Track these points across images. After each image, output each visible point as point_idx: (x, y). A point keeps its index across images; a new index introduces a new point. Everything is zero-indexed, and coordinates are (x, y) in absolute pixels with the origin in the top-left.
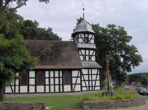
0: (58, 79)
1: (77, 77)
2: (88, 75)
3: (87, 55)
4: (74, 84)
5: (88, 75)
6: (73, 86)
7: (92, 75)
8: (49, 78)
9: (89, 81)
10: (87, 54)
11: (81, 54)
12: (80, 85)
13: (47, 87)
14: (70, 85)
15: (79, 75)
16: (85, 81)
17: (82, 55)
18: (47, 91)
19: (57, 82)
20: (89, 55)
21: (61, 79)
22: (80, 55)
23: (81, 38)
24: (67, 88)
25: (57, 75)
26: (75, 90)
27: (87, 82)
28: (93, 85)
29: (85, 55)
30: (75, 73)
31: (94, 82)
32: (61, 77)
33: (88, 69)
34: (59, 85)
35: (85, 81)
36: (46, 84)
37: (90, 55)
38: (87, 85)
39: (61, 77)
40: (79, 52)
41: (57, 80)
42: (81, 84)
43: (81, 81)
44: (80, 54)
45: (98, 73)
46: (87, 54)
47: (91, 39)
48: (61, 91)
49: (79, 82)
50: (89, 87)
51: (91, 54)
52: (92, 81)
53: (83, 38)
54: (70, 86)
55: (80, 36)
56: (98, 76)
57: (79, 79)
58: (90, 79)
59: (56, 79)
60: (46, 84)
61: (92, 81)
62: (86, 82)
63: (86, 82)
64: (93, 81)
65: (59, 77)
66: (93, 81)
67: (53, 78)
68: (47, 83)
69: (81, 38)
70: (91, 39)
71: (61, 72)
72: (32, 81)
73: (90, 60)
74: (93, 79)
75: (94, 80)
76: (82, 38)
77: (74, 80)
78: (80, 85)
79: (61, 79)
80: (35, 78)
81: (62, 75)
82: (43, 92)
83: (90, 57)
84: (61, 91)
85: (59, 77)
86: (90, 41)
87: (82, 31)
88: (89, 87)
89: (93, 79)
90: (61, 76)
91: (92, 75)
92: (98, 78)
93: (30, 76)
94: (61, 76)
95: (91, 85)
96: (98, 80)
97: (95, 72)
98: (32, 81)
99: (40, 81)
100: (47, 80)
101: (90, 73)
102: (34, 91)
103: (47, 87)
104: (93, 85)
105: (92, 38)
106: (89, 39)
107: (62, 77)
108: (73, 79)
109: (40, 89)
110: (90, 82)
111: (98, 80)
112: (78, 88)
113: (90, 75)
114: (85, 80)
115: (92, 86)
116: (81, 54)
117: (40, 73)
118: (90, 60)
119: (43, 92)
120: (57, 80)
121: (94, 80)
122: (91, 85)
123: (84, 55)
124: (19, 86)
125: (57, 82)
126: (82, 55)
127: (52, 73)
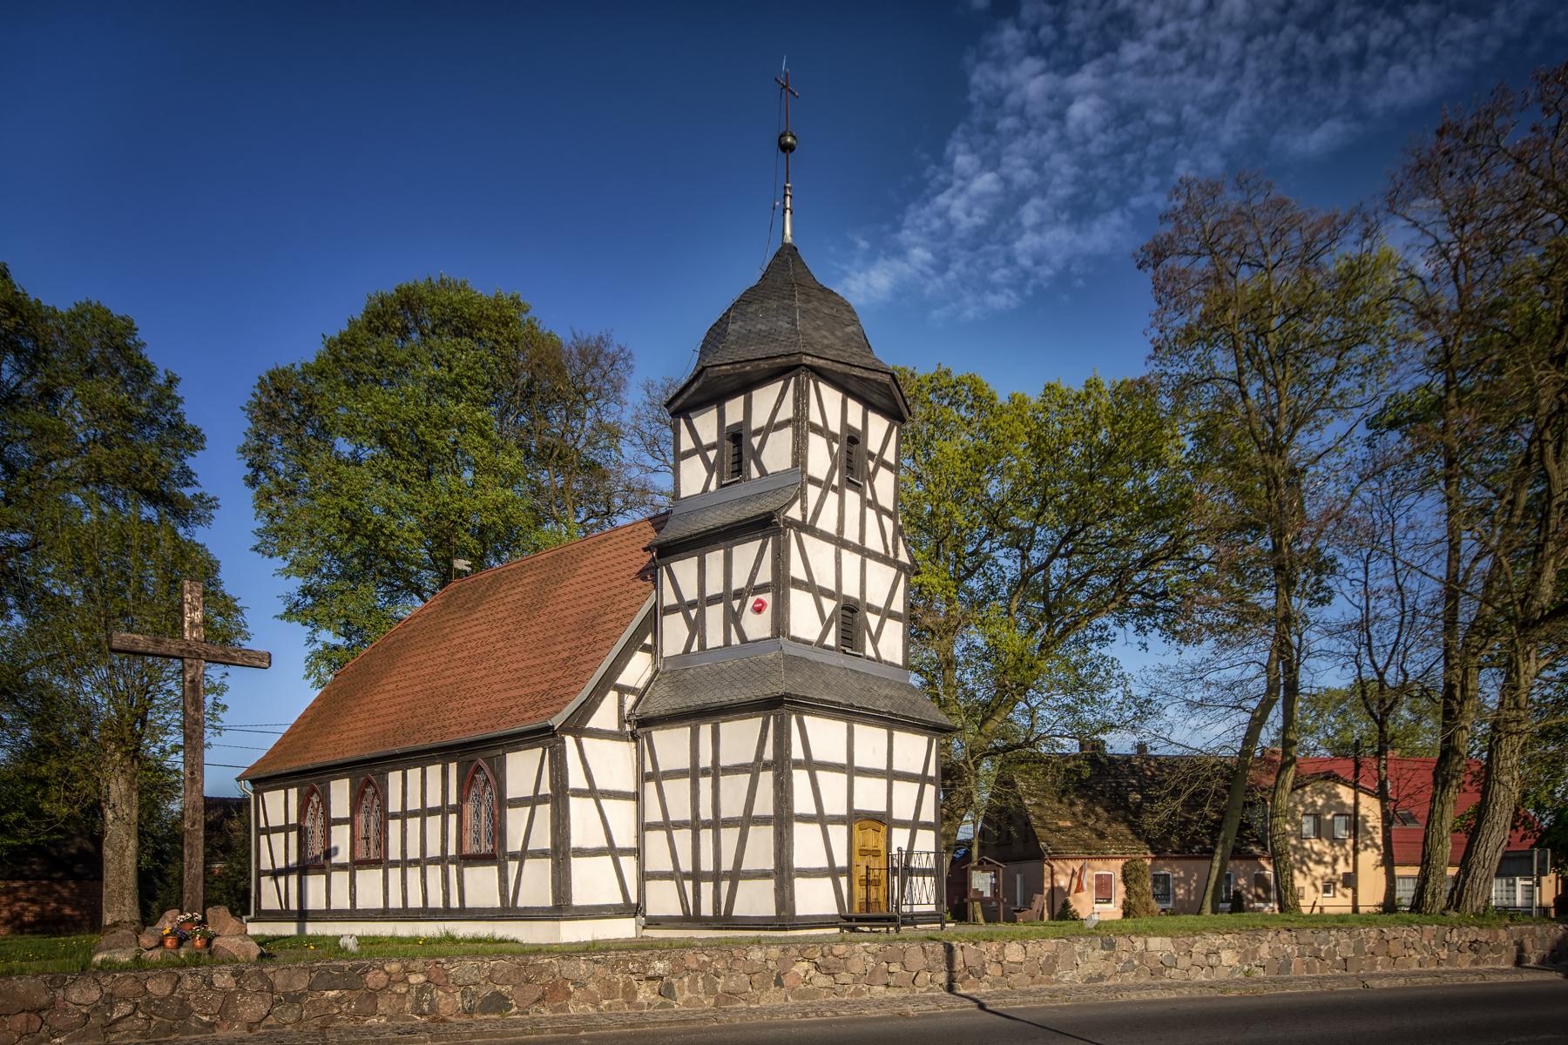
6: (513, 866)
15: (545, 789)
21: (453, 818)
37: (692, 604)
40: (657, 585)
69: (700, 449)
79: (453, 818)
90: (453, 800)
96: (924, 873)
111: (924, 873)
113: (707, 824)
118: (735, 640)
122: (707, 865)
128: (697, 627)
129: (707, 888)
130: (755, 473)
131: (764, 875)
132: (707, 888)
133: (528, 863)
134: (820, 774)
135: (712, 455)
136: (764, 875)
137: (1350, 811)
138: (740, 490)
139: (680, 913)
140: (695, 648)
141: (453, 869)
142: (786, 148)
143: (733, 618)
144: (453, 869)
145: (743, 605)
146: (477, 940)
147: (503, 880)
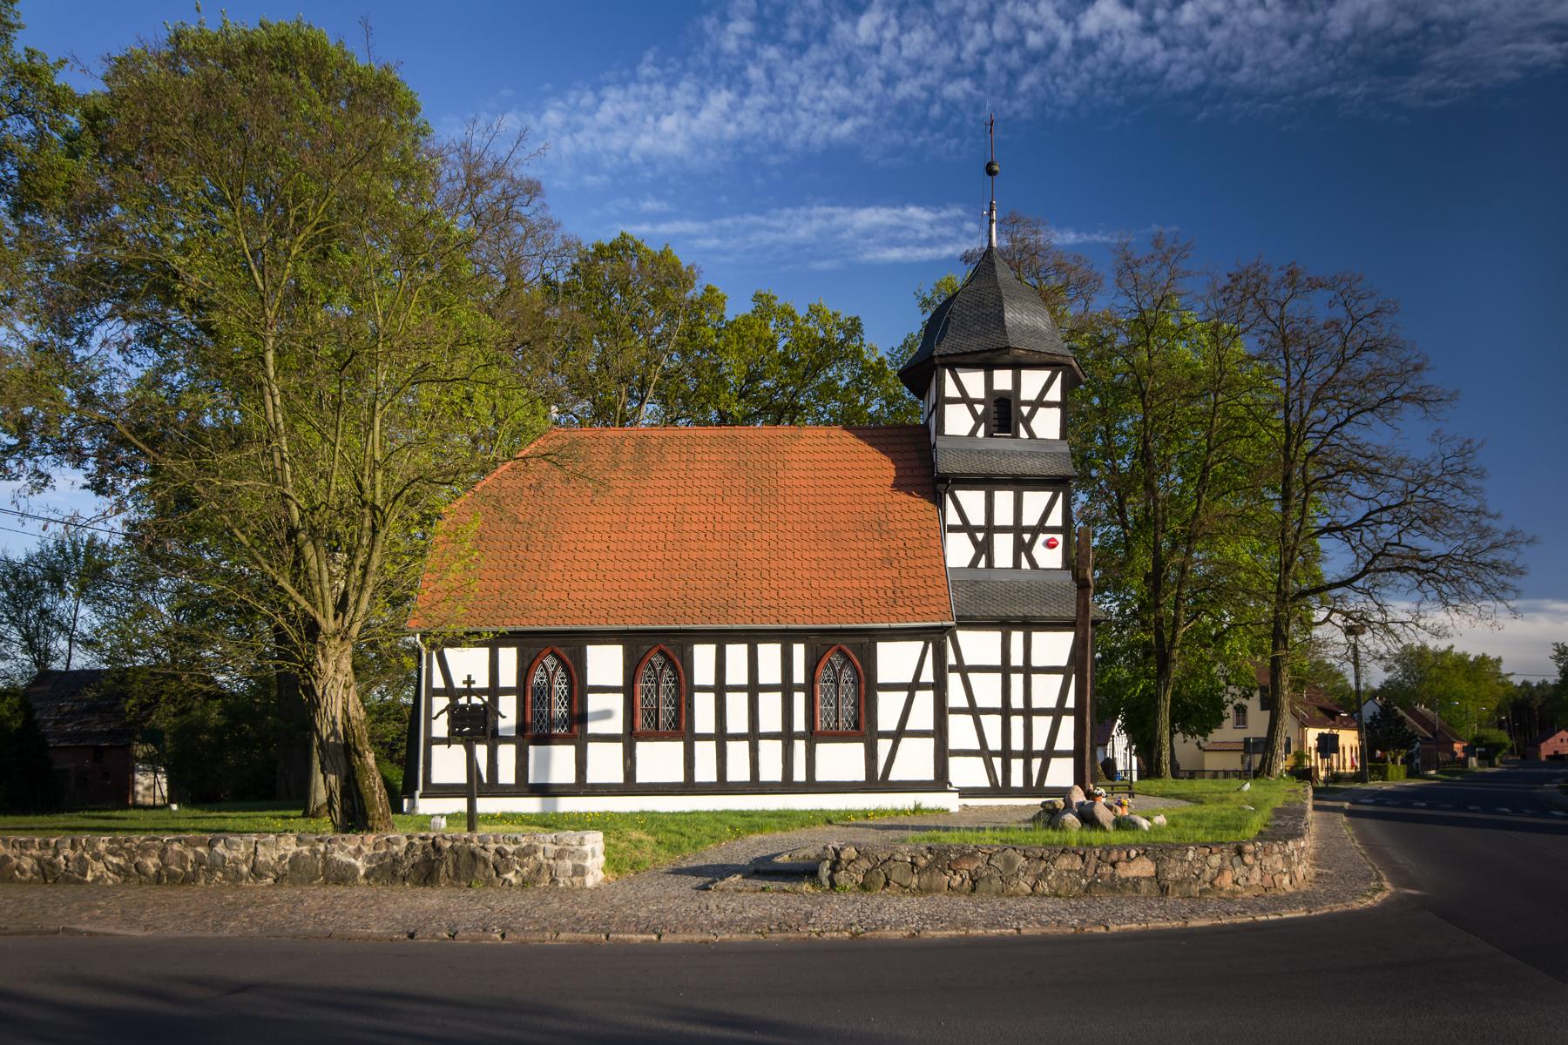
0: (711, 697)
1: (913, 687)
2: (1005, 669)
3: (1004, 529)
4: (886, 735)
5: (1005, 669)
6: (884, 746)
7: (1028, 670)
8: (720, 689)
9: (1006, 712)
10: (1004, 516)
11: (958, 522)
12: (930, 742)
13: (705, 753)
14: (572, 748)
15: (928, 676)
16: (974, 711)
17: (966, 527)
18: (706, 771)
19: (771, 720)
20: (1017, 529)
21: (799, 699)
22: (953, 529)
23: (965, 399)
24: (841, 760)
25: (770, 671)
26: (893, 777)
27: (992, 724)
28: (1039, 744)
29: (990, 528)
30: (897, 660)
31: (1041, 725)
32: (799, 688)
33: (1005, 625)
34: (787, 736)
35: (974, 711)
36: (698, 729)
38: (995, 743)
39: (799, 688)
40: (941, 505)
41: (770, 705)
42: (940, 732)
43: (942, 711)
44: (953, 518)
45: (1070, 703)
46: (1004, 516)
47: (1039, 403)
48: (799, 775)
49: (922, 715)
50: (1006, 754)
51: (1030, 518)
52: (1028, 712)
53: (979, 402)
54: (857, 750)
55: (951, 390)
56: (1068, 723)
57: (925, 700)
58: (1017, 702)
59: (730, 696)
60: (698, 729)
61: (1028, 712)
62: (965, 704)
63: (965, 704)
64: (1036, 719)
65: (786, 688)
66: (1036, 719)
67: (779, 695)
68: (704, 720)
69: (965, 399)
70: (1039, 403)
71: (799, 651)
72: (607, 713)
73: (1025, 564)
74: (1035, 705)
75: (1043, 712)
76: (970, 403)
77: (888, 709)
78: (952, 745)
79: (799, 699)
80: (628, 690)
81: (811, 670)
82: (679, 777)
83: (1027, 537)
84: (799, 775)
85: (786, 688)
86: (1027, 421)
87: (973, 344)
88: (1006, 754)
89: (1035, 705)
90: (799, 676)
91: (1028, 670)
92: (1066, 740)
93: (592, 679)
94: (799, 676)
95: (1017, 744)
97: (1054, 647)
98: (607, 713)
99: (660, 709)
100: (704, 706)
101: (1017, 659)
102: (618, 777)
103: (705, 753)
104: (1039, 744)
105: (1049, 397)
106: (1025, 410)
107: (809, 688)
108: (882, 696)
109: (660, 760)
110: (1017, 723)
112: (915, 760)
114: (980, 704)
115: (1028, 754)
116: (958, 522)
117: (659, 655)
118: (1025, 564)
119: (679, 777)
120: (770, 705)
121: (1043, 712)
122: (1017, 744)
123: (979, 529)
124: (629, 739)
125: (771, 720)
126: (966, 527)
127: (737, 654)
128: (984, 549)
129: (1017, 765)
130: (1023, 434)
131: (630, 771)
132: (1017, 765)
133: (905, 742)
134: (971, 676)
135: (980, 408)
136: (630, 771)
137: (406, 713)
138: (1003, 443)
139: (987, 784)
140: (982, 564)
141: (800, 747)
142: (990, 171)
143: (1022, 548)
144: (800, 747)
145: (1033, 541)
146: (865, 814)
147: (871, 756)
